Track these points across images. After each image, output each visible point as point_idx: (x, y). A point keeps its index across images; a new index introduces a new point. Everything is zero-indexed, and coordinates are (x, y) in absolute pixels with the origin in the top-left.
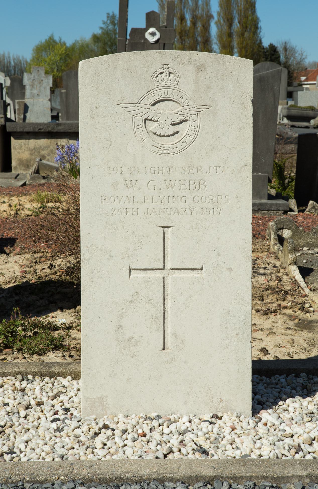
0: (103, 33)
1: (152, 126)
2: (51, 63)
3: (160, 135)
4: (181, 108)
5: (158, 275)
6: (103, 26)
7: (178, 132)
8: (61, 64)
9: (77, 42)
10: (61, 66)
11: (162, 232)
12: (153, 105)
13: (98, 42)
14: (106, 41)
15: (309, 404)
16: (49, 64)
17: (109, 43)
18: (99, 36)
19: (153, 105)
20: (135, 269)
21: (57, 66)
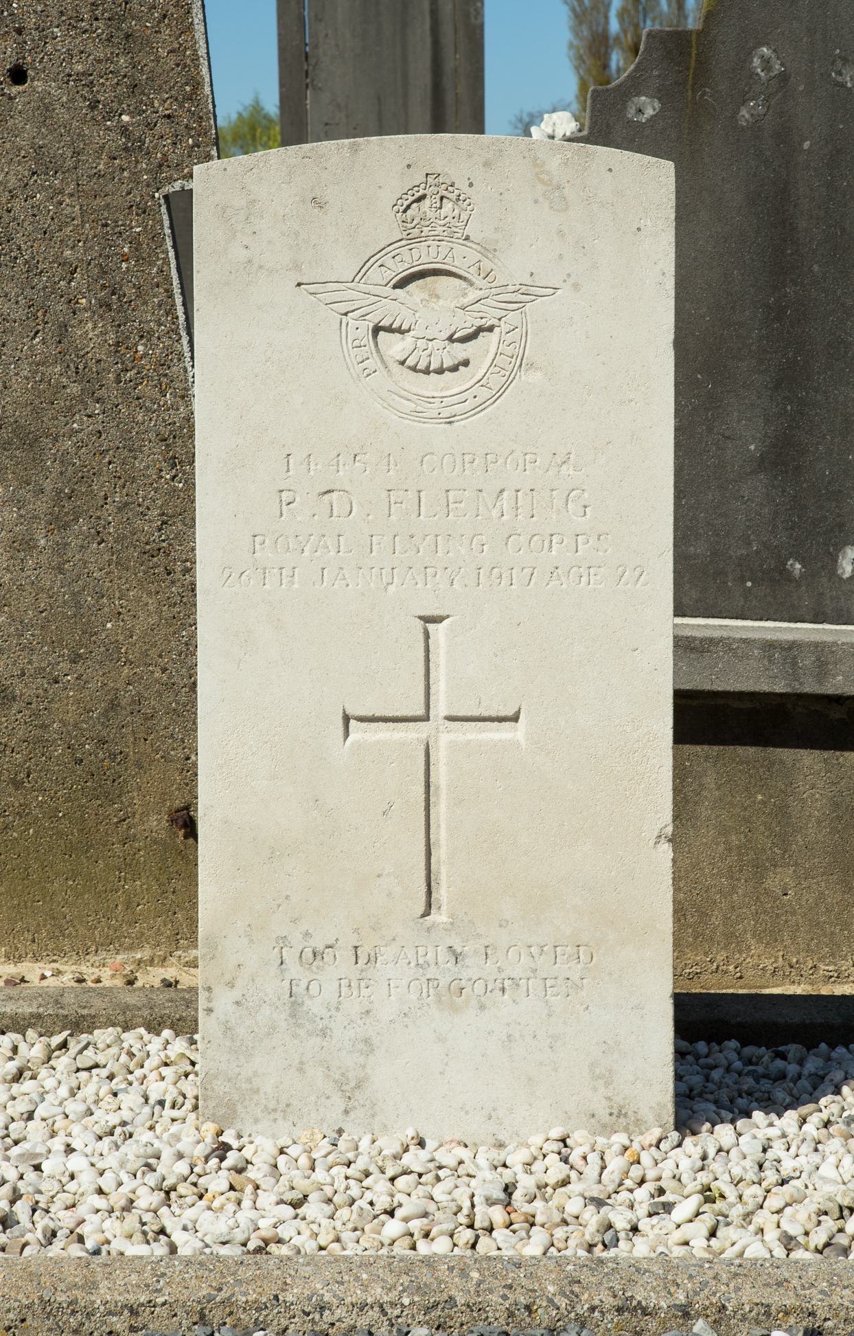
1: (394, 346)
3: (414, 369)
5: (412, 734)
9: (571, 46)
11: (421, 637)
19: (402, 284)
20: (362, 719)
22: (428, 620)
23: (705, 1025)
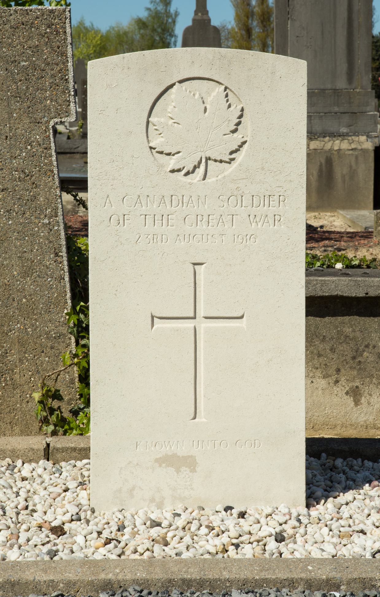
0: (150, 15)
5: (190, 324)
15: (371, 491)
18: (144, 20)
22: (195, 264)
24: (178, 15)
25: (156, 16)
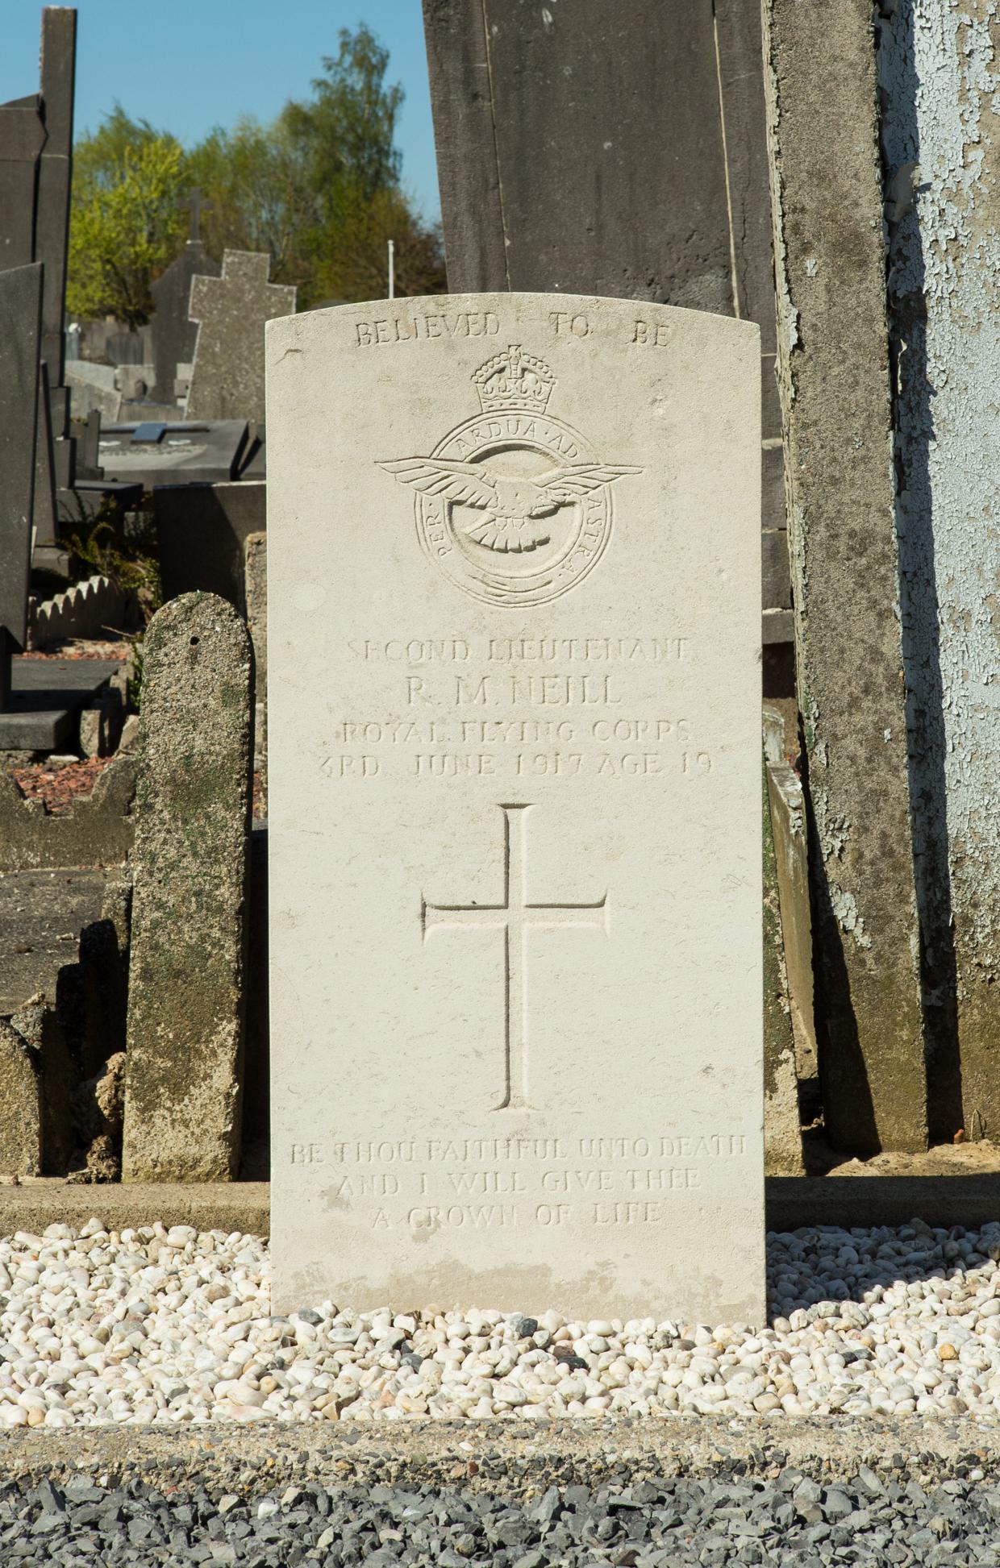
0: (327, 102)
2: (125, 211)
4: (556, 471)
5: (495, 922)
6: (327, 76)
7: (545, 541)
8: (164, 215)
10: (165, 223)
12: (477, 460)
13: (306, 133)
14: (339, 130)
16: (118, 214)
17: (351, 138)
18: (306, 109)
19: (477, 460)
21: (150, 219)
22: (505, 806)
23: (790, 1210)
24: (402, 98)
25: (339, 99)
